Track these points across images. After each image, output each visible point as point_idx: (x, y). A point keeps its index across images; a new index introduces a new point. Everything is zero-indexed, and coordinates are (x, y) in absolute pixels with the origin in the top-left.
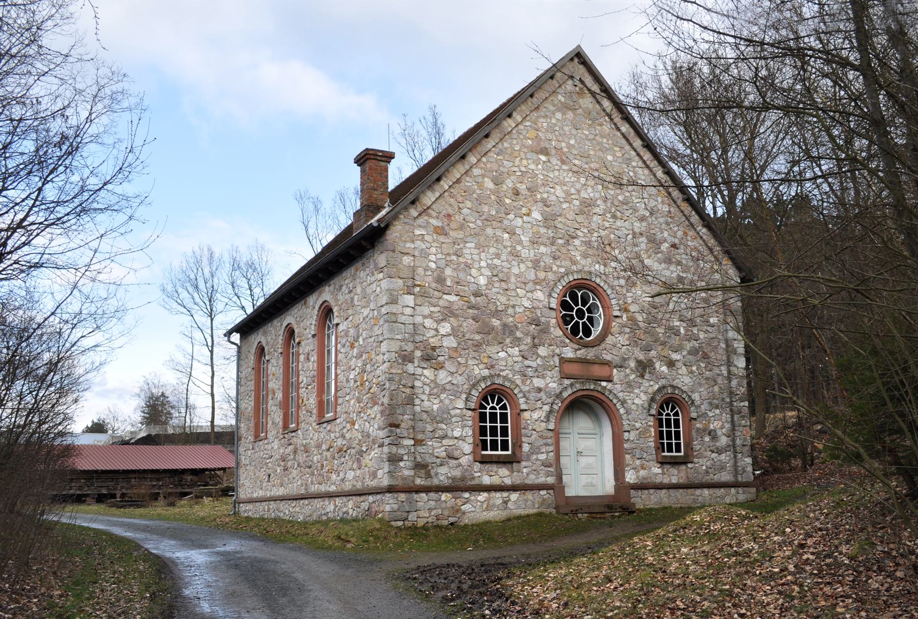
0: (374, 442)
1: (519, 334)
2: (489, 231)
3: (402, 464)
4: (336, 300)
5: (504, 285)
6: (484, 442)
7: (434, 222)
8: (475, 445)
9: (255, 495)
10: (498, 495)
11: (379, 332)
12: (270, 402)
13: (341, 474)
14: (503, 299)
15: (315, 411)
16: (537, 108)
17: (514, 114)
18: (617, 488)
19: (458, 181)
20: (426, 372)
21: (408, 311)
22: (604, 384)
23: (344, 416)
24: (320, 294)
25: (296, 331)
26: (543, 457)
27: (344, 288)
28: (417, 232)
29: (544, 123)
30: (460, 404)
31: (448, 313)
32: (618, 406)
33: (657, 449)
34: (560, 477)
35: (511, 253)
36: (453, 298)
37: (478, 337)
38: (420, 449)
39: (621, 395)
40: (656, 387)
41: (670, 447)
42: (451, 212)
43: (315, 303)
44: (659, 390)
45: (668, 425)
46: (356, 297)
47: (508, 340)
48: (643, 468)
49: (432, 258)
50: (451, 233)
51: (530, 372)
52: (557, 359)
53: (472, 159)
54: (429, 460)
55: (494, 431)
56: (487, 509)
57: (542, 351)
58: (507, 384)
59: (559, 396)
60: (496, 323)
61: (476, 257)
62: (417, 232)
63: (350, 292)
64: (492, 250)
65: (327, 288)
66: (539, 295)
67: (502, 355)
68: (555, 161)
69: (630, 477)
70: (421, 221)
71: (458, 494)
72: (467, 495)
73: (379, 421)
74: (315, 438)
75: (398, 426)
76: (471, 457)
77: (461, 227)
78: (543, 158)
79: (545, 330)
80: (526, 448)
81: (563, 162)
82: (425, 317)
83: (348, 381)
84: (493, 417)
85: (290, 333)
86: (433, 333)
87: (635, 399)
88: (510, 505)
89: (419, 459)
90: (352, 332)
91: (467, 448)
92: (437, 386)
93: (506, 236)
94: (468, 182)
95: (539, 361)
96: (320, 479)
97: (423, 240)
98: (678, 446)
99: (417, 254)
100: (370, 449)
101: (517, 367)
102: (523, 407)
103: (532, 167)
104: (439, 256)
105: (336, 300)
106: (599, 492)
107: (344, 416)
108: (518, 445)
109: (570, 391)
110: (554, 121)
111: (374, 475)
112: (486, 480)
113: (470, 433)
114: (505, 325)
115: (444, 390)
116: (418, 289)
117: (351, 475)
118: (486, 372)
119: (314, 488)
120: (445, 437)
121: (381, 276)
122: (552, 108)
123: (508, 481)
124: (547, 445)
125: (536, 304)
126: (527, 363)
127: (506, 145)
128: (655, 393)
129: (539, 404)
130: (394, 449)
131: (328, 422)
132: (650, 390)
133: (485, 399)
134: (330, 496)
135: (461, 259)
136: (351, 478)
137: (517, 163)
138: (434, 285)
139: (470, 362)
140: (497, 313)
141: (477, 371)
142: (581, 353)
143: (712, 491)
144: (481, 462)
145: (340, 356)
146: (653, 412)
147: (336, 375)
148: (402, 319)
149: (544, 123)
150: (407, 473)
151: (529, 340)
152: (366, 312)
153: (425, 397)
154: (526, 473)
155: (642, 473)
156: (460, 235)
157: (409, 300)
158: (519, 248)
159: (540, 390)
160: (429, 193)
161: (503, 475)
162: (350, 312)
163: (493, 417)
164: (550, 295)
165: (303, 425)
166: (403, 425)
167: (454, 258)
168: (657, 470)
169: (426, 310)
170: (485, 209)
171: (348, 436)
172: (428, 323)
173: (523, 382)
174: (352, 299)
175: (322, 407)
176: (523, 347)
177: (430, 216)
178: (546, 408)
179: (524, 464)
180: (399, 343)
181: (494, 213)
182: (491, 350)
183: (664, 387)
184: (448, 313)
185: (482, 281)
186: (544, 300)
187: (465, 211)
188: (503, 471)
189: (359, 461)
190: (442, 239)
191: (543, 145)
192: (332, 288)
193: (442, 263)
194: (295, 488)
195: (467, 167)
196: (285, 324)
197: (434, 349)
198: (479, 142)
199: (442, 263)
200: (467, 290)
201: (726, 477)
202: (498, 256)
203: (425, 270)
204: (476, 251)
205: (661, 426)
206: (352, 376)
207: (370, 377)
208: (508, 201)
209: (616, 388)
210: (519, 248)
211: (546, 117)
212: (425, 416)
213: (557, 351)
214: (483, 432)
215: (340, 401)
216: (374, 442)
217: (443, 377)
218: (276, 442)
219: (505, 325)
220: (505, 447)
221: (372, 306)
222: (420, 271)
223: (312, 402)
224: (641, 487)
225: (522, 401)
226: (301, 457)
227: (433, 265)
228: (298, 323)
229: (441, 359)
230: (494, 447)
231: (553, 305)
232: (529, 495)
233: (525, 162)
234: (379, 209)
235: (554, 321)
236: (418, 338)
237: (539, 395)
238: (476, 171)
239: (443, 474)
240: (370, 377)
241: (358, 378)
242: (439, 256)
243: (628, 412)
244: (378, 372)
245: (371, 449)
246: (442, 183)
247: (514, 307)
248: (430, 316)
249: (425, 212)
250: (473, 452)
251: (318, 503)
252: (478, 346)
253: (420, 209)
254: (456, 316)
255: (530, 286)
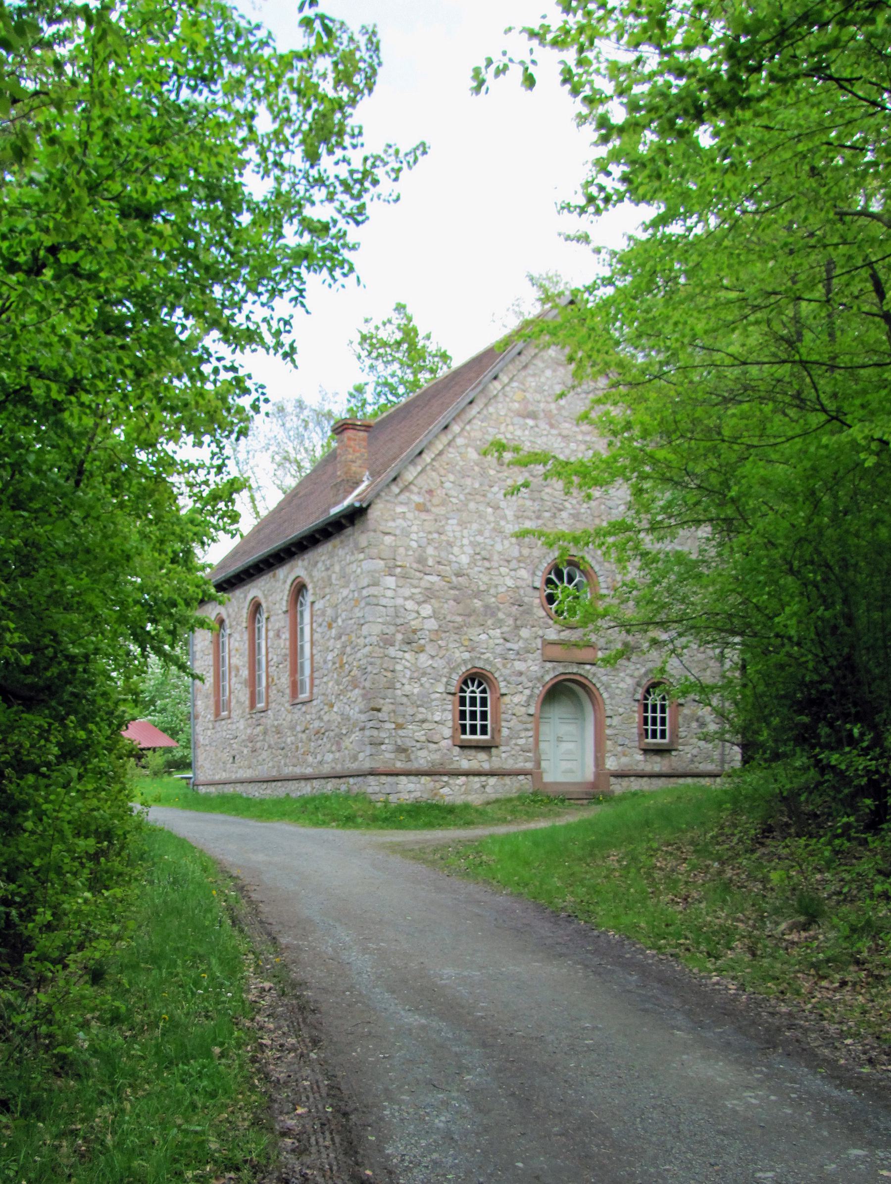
0: (354, 725)
1: (501, 615)
2: (472, 506)
3: (383, 747)
4: (311, 577)
5: (487, 564)
6: (464, 727)
7: (416, 498)
8: (455, 730)
9: (217, 777)
10: (476, 779)
11: (360, 615)
12: (234, 680)
13: (319, 757)
14: (485, 579)
15: (288, 691)
16: (525, 367)
17: (501, 376)
18: (597, 775)
19: (441, 453)
20: (407, 656)
21: (389, 593)
22: (588, 667)
23: (321, 698)
24: (292, 570)
25: (264, 605)
26: (521, 742)
27: (320, 565)
28: (399, 509)
29: (531, 382)
30: (441, 688)
31: (429, 595)
32: (602, 690)
33: (640, 735)
34: (538, 764)
35: (494, 529)
36: (434, 578)
37: (459, 619)
38: (401, 732)
39: (604, 678)
40: (643, 670)
41: (654, 732)
42: (433, 486)
43: (287, 577)
44: (646, 674)
45: (654, 710)
46: (334, 576)
47: (490, 622)
48: (625, 755)
49: (414, 536)
50: (433, 509)
51: (511, 655)
52: (539, 641)
53: (456, 428)
54: (409, 743)
55: (473, 715)
56: (465, 793)
57: (525, 633)
58: (488, 667)
59: (540, 679)
60: (477, 603)
61: (458, 534)
62: (399, 509)
63: (327, 569)
64: (475, 526)
65: (300, 563)
66: (523, 573)
67: (484, 637)
68: (543, 425)
69: (611, 764)
70: (403, 497)
71: (436, 778)
72: (445, 779)
73: (361, 705)
74: (289, 717)
75: (379, 710)
76: (450, 742)
77: (443, 504)
78: (531, 422)
79: (529, 612)
80: (505, 732)
81: (552, 426)
82: (406, 599)
83: (325, 662)
84: (473, 701)
85: (256, 607)
86: (415, 615)
87: (619, 687)
88: (488, 789)
89: (399, 743)
90: (329, 611)
91: (447, 732)
92: (418, 669)
93: (490, 510)
94: (452, 454)
95: (521, 644)
96: (295, 761)
97: (404, 518)
98: (663, 733)
99: (398, 532)
100: (350, 732)
101: (499, 650)
102: (503, 691)
103: (518, 433)
104: (421, 534)
105: (311, 577)
106: (576, 778)
107: (321, 698)
108: (497, 730)
109: (552, 675)
110: (543, 380)
111: (355, 758)
112: (465, 765)
113: (450, 717)
114: (487, 607)
115: (424, 674)
116: (399, 570)
117: (329, 757)
118: (466, 655)
119: (288, 771)
120: (423, 721)
121: (362, 556)
122: (541, 365)
123: (486, 766)
124: (527, 730)
125: (520, 583)
126: (509, 645)
127: (491, 409)
128: (641, 677)
129: (520, 688)
130: (375, 733)
131: (303, 703)
132: (636, 674)
133: (465, 683)
134: (307, 778)
135: (443, 537)
136: (330, 761)
137: (503, 429)
138: (415, 566)
139: (451, 646)
140: (478, 594)
141: (457, 654)
142: (566, 635)
143: (696, 780)
144: (461, 747)
145: (316, 636)
146: (639, 696)
147: (312, 656)
148: (383, 601)
149: (531, 382)
150: (388, 755)
151: (511, 621)
152: (345, 592)
153: (404, 681)
154: (502, 759)
155: (624, 760)
156: (442, 511)
157: (390, 581)
158: (502, 523)
159: (521, 674)
160: (411, 468)
161: (480, 760)
162: (327, 590)
163: (473, 701)
164: (534, 574)
165: (273, 705)
166: (384, 709)
167: (436, 536)
168: (640, 757)
169: (407, 592)
170: (468, 481)
171: (326, 718)
172: (410, 605)
173: (504, 666)
174: (330, 577)
175: (295, 687)
176: (505, 629)
177: (411, 492)
178: (527, 692)
179: (502, 748)
180: (380, 627)
181: (477, 486)
182: (473, 633)
183: (651, 671)
184: (429, 595)
185: (464, 560)
186: (529, 578)
187: (448, 485)
188: (482, 756)
189: (338, 743)
190: (424, 516)
191: (531, 408)
192: (306, 563)
193: (424, 542)
194: (265, 770)
195: (450, 437)
196: (250, 597)
197: (414, 632)
198: (463, 410)
199: (424, 542)
200: (447, 570)
201: (710, 767)
202: (480, 533)
203: (407, 550)
204: (458, 528)
205: (646, 711)
206: (330, 657)
207: (350, 659)
208: (492, 472)
209: (599, 676)
210: (502, 523)
211: (534, 375)
212: (405, 700)
213: (540, 633)
214: (463, 715)
215: (317, 682)
216: (354, 725)
217: (424, 660)
218: (242, 721)
219: (487, 607)
220: (484, 731)
221: (352, 586)
222: (402, 550)
223: (285, 681)
224: (620, 775)
225: (502, 684)
226: (272, 739)
227: (414, 545)
228: (266, 597)
229: (422, 642)
230: (473, 731)
231: (537, 584)
232: (507, 780)
233: (511, 428)
234: (357, 484)
235: (537, 601)
236: (399, 621)
237: (520, 679)
238: (460, 441)
239: (423, 759)
240: (350, 659)
241: (337, 660)
242: (421, 534)
243: (611, 697)
244: (359, 655)
245: (352, 732)
246: (424, 455)
247: (496, 586)
248: (411, 597)
249: (406, 488)
250: (453, 737)
251: (292, 786)
252: (458, 630)
253: (401, 485)
254: (437, 597)
255: (514, 565)
